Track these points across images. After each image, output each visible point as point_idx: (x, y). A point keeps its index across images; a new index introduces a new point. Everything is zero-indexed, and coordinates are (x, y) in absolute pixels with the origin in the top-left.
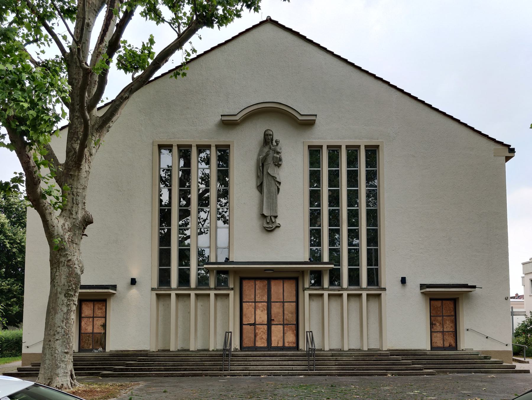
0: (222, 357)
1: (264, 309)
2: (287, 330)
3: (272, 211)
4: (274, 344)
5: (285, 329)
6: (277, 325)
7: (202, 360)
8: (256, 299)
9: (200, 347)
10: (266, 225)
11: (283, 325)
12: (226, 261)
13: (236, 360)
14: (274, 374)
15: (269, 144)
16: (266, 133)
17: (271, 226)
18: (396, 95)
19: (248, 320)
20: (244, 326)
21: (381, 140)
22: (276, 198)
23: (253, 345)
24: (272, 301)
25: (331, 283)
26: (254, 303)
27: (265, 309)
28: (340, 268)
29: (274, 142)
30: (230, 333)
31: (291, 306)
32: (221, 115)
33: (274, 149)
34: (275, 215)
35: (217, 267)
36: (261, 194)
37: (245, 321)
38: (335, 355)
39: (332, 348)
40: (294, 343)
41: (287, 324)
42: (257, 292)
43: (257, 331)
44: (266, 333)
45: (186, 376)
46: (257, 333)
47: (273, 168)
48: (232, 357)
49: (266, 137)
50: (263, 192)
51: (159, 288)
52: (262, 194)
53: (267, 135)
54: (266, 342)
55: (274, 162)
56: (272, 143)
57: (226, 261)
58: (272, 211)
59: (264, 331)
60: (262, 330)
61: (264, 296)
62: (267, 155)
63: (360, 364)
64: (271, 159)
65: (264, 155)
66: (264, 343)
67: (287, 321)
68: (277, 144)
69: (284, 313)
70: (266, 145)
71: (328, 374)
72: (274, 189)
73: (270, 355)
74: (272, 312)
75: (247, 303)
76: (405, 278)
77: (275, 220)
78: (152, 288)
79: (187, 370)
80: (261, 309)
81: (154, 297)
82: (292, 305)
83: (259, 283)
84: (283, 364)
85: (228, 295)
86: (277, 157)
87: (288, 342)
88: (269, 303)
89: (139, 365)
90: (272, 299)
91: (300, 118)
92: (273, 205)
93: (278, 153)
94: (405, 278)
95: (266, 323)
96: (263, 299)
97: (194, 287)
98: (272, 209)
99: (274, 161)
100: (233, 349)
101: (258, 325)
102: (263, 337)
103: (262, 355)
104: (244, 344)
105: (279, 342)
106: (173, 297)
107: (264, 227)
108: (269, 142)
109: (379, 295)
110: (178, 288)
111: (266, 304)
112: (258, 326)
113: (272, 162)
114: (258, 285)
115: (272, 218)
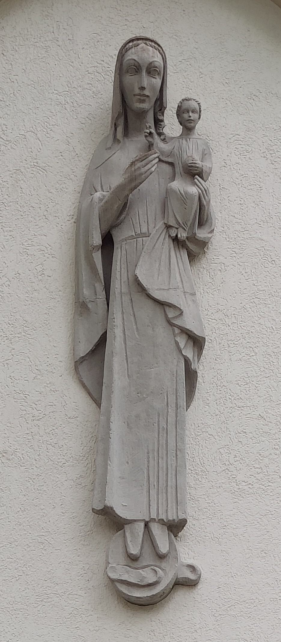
3: (153, 492)
15: (139, 130)
16: (131, 55)
17: (151, 578)
22: (179, 423)
34: (172, 516)
36: (98, 402)
49: (129, 79)
50: (110, 386)
52: (99, 405)
53: (137, 68)
55: (168, 227)
56: (158, 122)
77: (171, 543)
86: (184, 199)
92: (162, 463)
99: (172, 222)
107: (112, 581)
113: (160, 224)
115: (157, 530)
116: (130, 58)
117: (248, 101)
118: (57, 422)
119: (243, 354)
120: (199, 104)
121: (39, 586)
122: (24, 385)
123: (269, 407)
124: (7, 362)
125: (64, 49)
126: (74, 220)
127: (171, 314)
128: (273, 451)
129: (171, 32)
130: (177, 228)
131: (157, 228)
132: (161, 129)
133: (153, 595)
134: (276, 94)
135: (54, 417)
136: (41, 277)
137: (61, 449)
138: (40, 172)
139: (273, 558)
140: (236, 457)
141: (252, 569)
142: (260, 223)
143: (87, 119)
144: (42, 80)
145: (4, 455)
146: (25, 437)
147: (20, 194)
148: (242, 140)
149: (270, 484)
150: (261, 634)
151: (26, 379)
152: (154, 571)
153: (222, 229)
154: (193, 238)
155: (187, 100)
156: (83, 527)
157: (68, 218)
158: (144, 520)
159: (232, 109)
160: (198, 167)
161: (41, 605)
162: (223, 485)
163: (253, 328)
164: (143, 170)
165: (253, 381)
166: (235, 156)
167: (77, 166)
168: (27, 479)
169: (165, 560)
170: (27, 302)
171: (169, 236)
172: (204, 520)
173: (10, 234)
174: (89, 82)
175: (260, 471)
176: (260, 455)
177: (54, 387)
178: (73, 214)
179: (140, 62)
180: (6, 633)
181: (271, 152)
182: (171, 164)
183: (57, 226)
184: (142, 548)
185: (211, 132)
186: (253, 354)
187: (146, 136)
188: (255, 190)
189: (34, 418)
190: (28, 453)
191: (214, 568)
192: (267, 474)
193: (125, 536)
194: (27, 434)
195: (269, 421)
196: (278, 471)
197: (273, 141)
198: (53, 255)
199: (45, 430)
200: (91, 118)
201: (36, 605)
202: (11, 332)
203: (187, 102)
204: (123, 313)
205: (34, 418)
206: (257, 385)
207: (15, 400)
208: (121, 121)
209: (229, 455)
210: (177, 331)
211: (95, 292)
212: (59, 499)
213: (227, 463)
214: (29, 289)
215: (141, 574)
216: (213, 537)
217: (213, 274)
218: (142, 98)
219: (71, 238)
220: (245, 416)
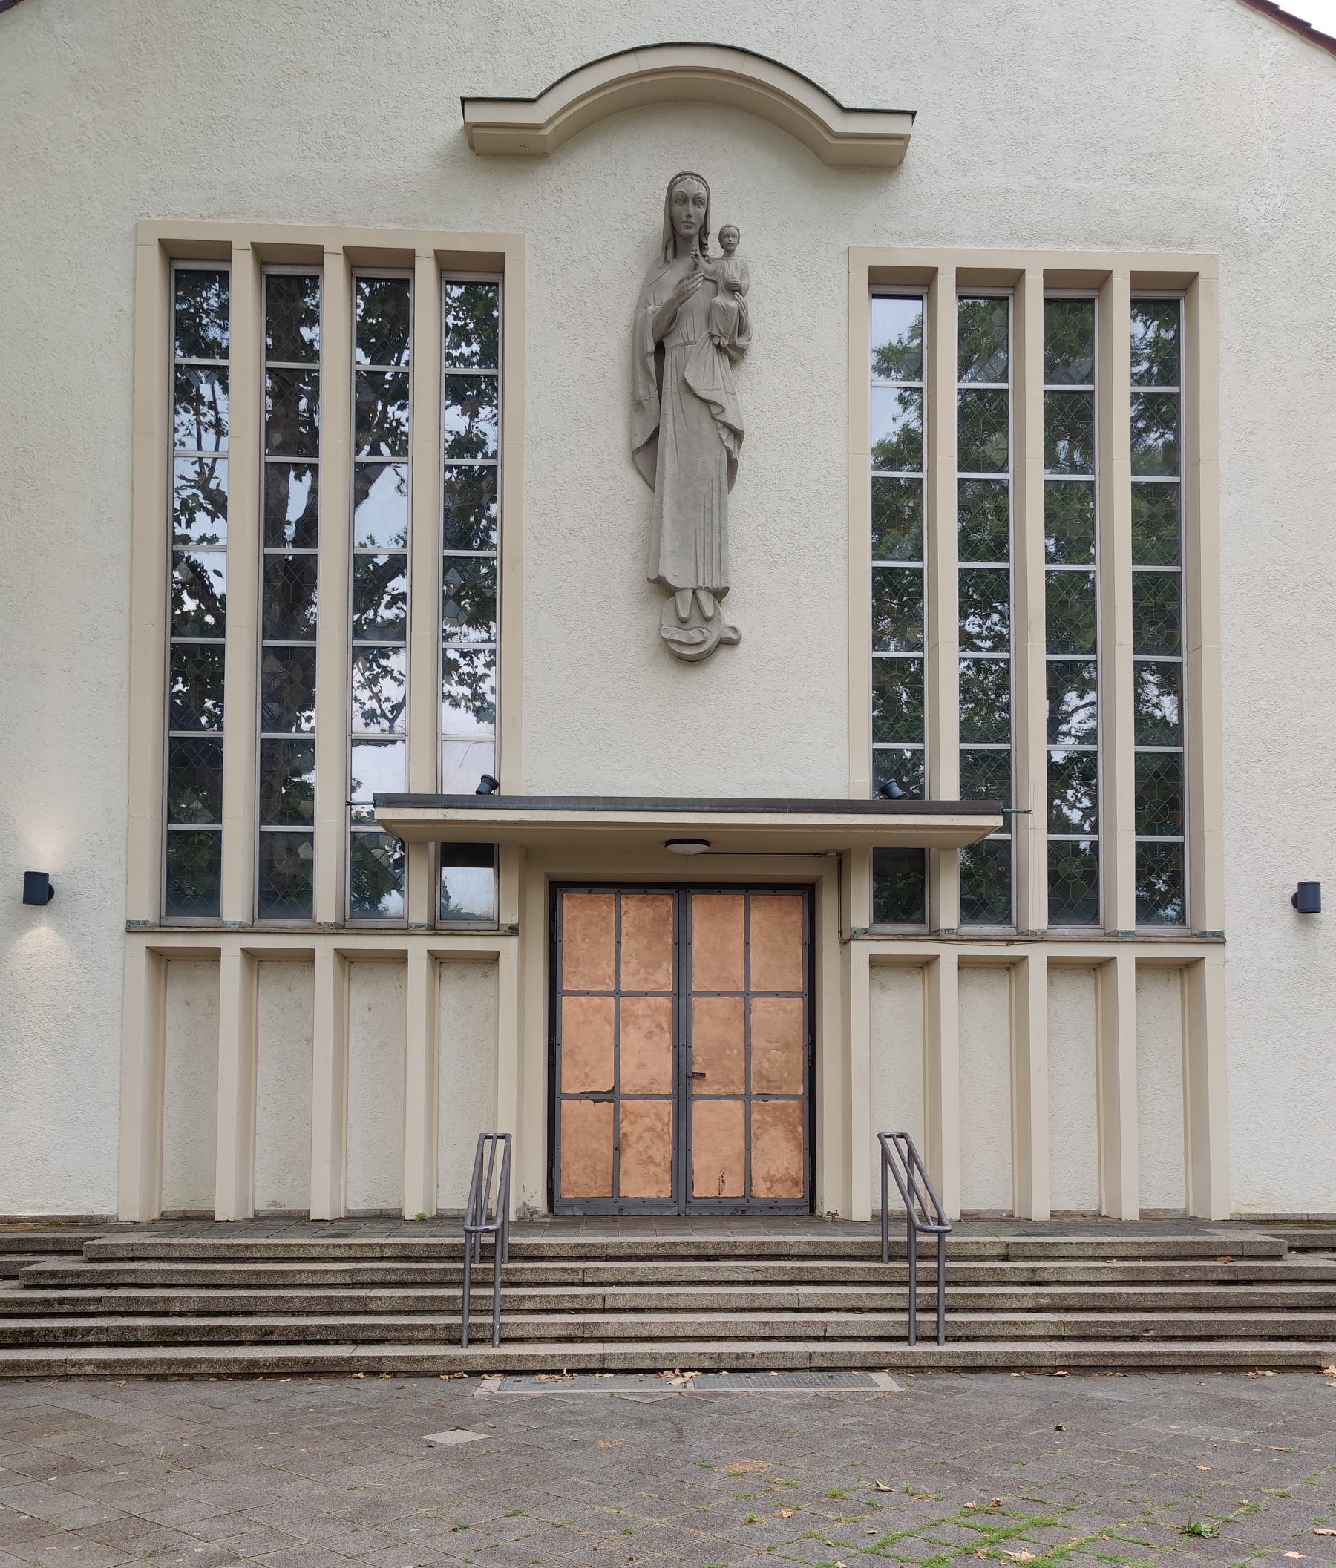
0: (462, 1259)
1: (659, 1026)
2: (763, 1122)
4: (704, 1187)
5: (755, 1116)
6: (719, 1097)
7: (359, 1278)
8: (624, 978)
9: (359, 1202)
10: (673, 633)
11: (747, 1098)
12: (482, 790)
13: (530, 1277)
14: (735, 1364)
15: (687, 253)
16: (680, 188)
18: (1274, 50)
19: (587, 1075)
20: (564, 1102)
21: (1202, 249)
22: (722, 505)
23: (606, 1191)
24: (695, 989)
25: (973, 908)
26: (611, 1000)
27: (665, 1026)
28: (1010, 841)
30: (501, 1143)
31: (781, 1015)
32: (464, 100)
33: (714, 273)
34: (716, 584)
35: (441, 817)
36: (652, 486)
37: (570, 1081)
38: (1019, 1253)
39: (971, 1207)
40: (796, 1184)
41: (765, 1097)
42: (628, 946)
43: (625, 1127)
44: (668, 1138)
45: (266, 1375)
46: (625, 1135)
47: (709, 362)
48: (512, 1258)
51: (164, 922)
52: (653, 489)
53: (684, 199)
54: (667, 1177)
55: (712, 336)
56: (703, 246)
57: (484, 790)
59: (659, 1126)
60: (647, 1120)
61: (659, 966)
62: (682, 296)
63: (1161, 1304)
64: (700, 319)
65: (667, 295)
66: (657, 1181)
67: (765, 1084)
68: (728, 250)
69: (748, 1046)
70: (675, 255)
71: (1019, 1363)
72: (713, 460)
73: (702, 1252)
74: (697, 1042)
75: (583, 999)
76: (1316, 885)
77: (715, 608)
78: (129, 923)
79: (274, 1338)
80: (646, 1024)
81: (140, 965)
82: (785, 1011)
83: (634, 909)
84: (774, 1304)
85: (492, 959)
86: (725, 312)
87: (770, 1179)
88: (683, 1000)
89: (22, 1310)
90: (695, 981)
91: (840, 124)
92: (708, 539)
93: (734, 289)
94: (1316, 885)
95: (667, 1090)
96: (656, 981)
97: (332, 920)
99: (715, 332)
100: (517, 1211)
101: (629, 1097)
102: (652, 1152)
103: (661, 1251)
104: (564, 1185)
105: (727, 1178)
106: (231, 965)
107: (665, 640)
108: (689, 238)
109: (1190, 966)
110: (257, 923)
111: (666, 1003)
112: (628, 1103)
113: (705, 334)
114: (632, 914)
115: (703, 596)
164: (690, 287)
182: (714, 282)
210: (720, 425)
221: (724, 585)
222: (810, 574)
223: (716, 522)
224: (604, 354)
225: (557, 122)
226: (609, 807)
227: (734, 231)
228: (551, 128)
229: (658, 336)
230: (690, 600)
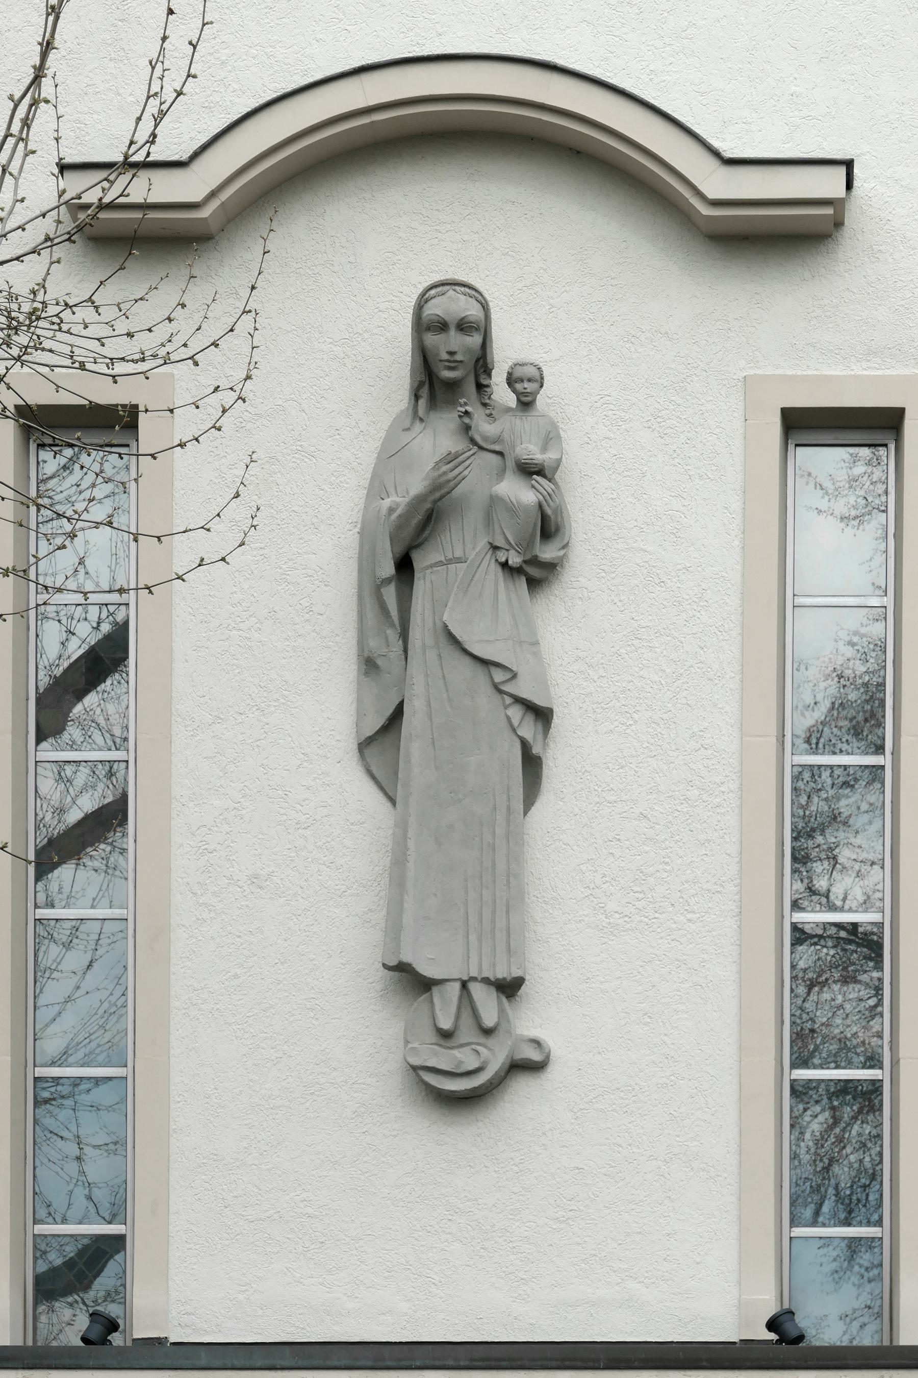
3: (473, 938)
12: (92, 1336)
15: (452, 402)
16: (436, 308)
17: (472, 1063)
29: (498, 379)
33: (498, 440)
34: (501, 972)
53: (442, 326)
58: (473, 938)
77: (502, 1011)
91: (706, 211)
98: (473, 919)
99: (500, 542)
107: (415, 1068)
116: (432, 312)
117: (623, 344)
118: (334, 830)
119: (616, 723)
120: (539, 368)
121: (308, 1072)
122: (283, 778)
123: (655, 801)
124: (258, 743)
125: (342, 277)
126: (357, 530)
127: (499, 676)
128: (661, 866)
129: (506, 246)
130: (507, 550)
131: (477, 550)
132: (486, 397)
133: (475, 1088)
134: (667, 333)
135: (329, 823)
136: (308, 615)
137: (341, 870)
138: (307, 460)
139: (661, 1024)
140: (604, 876)
141: (629, 1042)
142: (642, 526)
143: (378, 379)
144: (309, 324)
145: (254, 880)
146: (285, 853)
147: (277, 494)
148: (614, 403)
149: (657, 915)
150: (644, 1137)
151: (287, 768)
152: (475, 1053)
153: (585, 536)
154: (534, 561)
155: (520, 365)
156: (374, 984)
157: (349, 527)
158: (460, 979)
159: (600, 357)
160: (536, 464)
161: (311, 1101)
162: (586, 919)
163: (631, 683)
164: (451, 475)
165: (631, 763)
166: (603, 427)
167: (362, 449)
168: (289, 915)
169: (493, 1035)
170: (287, 653)
171: (497, 560)
172: (557, 971)
173: (261, 552)
174: (380, 324)
175: (640, 896)
176: (642, 872)
177: (329, 779)
178: (355, 520)
179: (446, 319)
180: (259, 1142)
181: (659, 420)
182: (500, 454)
183: (332, 539)
184: (458, 1017)
185: (567, 392)
186: (632, 722)
187: (460, 417)
188: (634, 476)
189: (298, 826)
190: (290, 878)
191: (572, 1040)
192: (652, 900)
193: (432, 1002)
194: (289, 849)
195: (656, 821)
196: (669, 896)
197: (662, 403)
198: (326, 583)
199: (316, 843)
200: (384, 378)
201: (303, 1101)
202: (263, 699)
203: (520, 367)
204: (427, 675)
205: (298, 826)
206: (636, 769)
207: (270, 800)
208: (425, 392)
209: (595, 874)
210: (508, 700)
211: (387, 641)
212: (337, 944)
213: (592, 886)
214: (289, 633)
215: (456, 1057)
216: (570, 995)
217: (570, 604)
218: (452, 365)
219: (353, 556)
220: (619, 816)
221: (516, 973)
222: (673, 944)
223: (501, 866)
224: (310, 572)
225: (225, 195)
226: (300, 1363)
227: (531, 371)
228: (214, 205)
229: (400, 549)
230: (455, 1000)
